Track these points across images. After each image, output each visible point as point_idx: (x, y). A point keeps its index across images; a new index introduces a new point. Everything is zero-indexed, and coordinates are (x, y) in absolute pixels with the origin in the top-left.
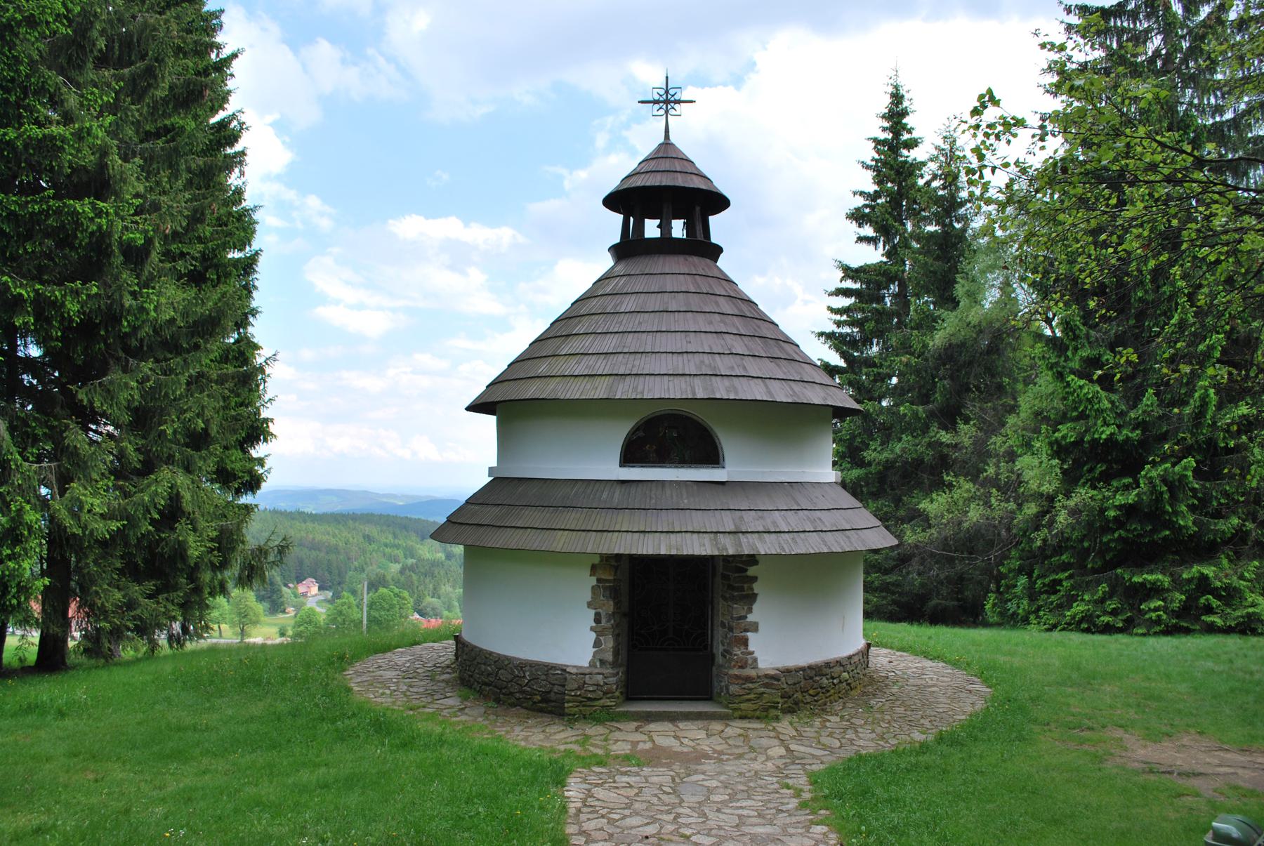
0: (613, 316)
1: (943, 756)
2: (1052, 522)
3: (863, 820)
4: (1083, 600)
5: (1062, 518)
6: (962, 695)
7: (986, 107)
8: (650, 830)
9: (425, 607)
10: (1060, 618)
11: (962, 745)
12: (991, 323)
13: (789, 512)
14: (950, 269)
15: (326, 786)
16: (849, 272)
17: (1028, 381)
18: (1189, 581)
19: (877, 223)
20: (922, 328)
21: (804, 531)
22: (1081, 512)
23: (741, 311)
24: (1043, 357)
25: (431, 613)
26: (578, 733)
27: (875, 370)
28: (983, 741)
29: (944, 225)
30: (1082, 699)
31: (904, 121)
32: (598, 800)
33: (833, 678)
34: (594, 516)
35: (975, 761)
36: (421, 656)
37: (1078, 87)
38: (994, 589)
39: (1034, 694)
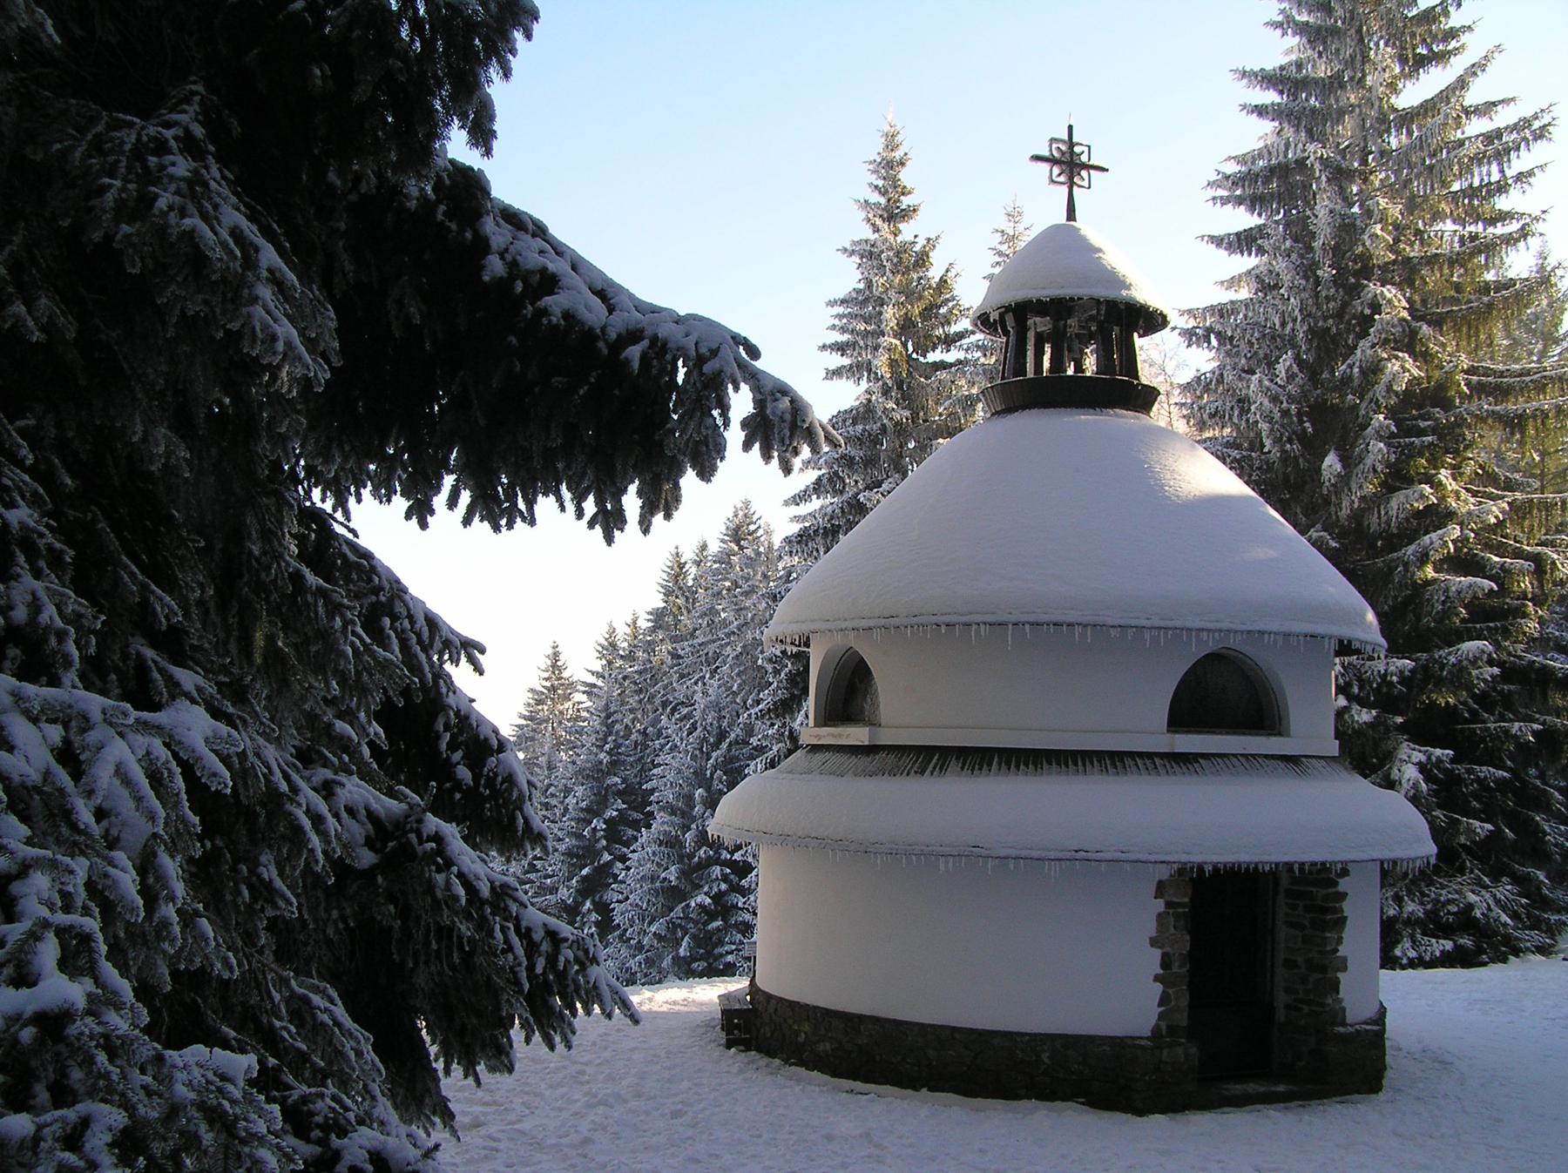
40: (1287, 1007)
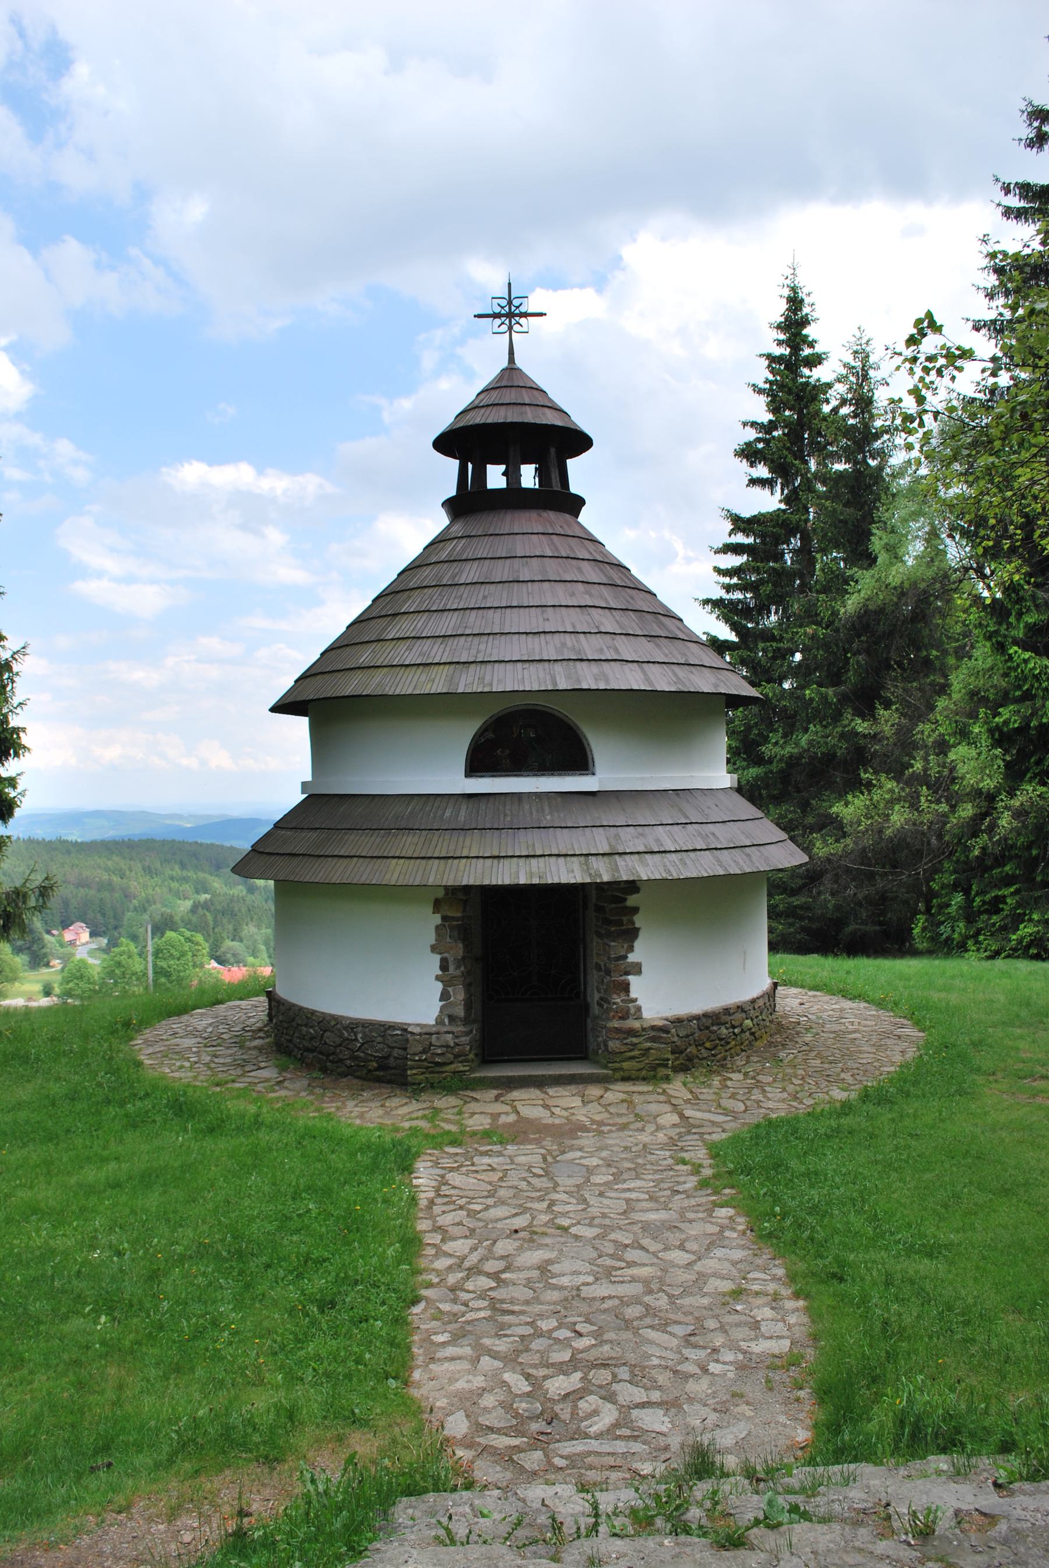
0: (450, 589)
1: (869, 1117)
2: (992, 828)
3: (776, 1199)
4: (1031, 920)
5: (1005, 821)
6: (889, 1042)
7: (925, 335)
8: (520, 1222)
9: (225, 953)
10: (1004, 943)
11: (892, 1102)
12: (915, 583)
13: (675, 827)
14: (864, 517)
15: (117, 1185)
16: (740, 524)
17: (962, 654)
19: (772, 461)
20: (831, 591)
21: (695, 850)
22: (1027, 813)
23: (611, 578)
24: (980, 624)
25: (232, 960)
26: (424, 1106)
27: (774, 644)
28: (917, 1097)
29: (856, 462)
30: (1034, 1042)
31: (804, 332)
32: (454, 1187)
33: (734, 1027)
34: (435, 838)
35: (907, 1122)
36: (225, 1018)
37: (1040, 311)
38: (923, 909)
39: (976, 1037)
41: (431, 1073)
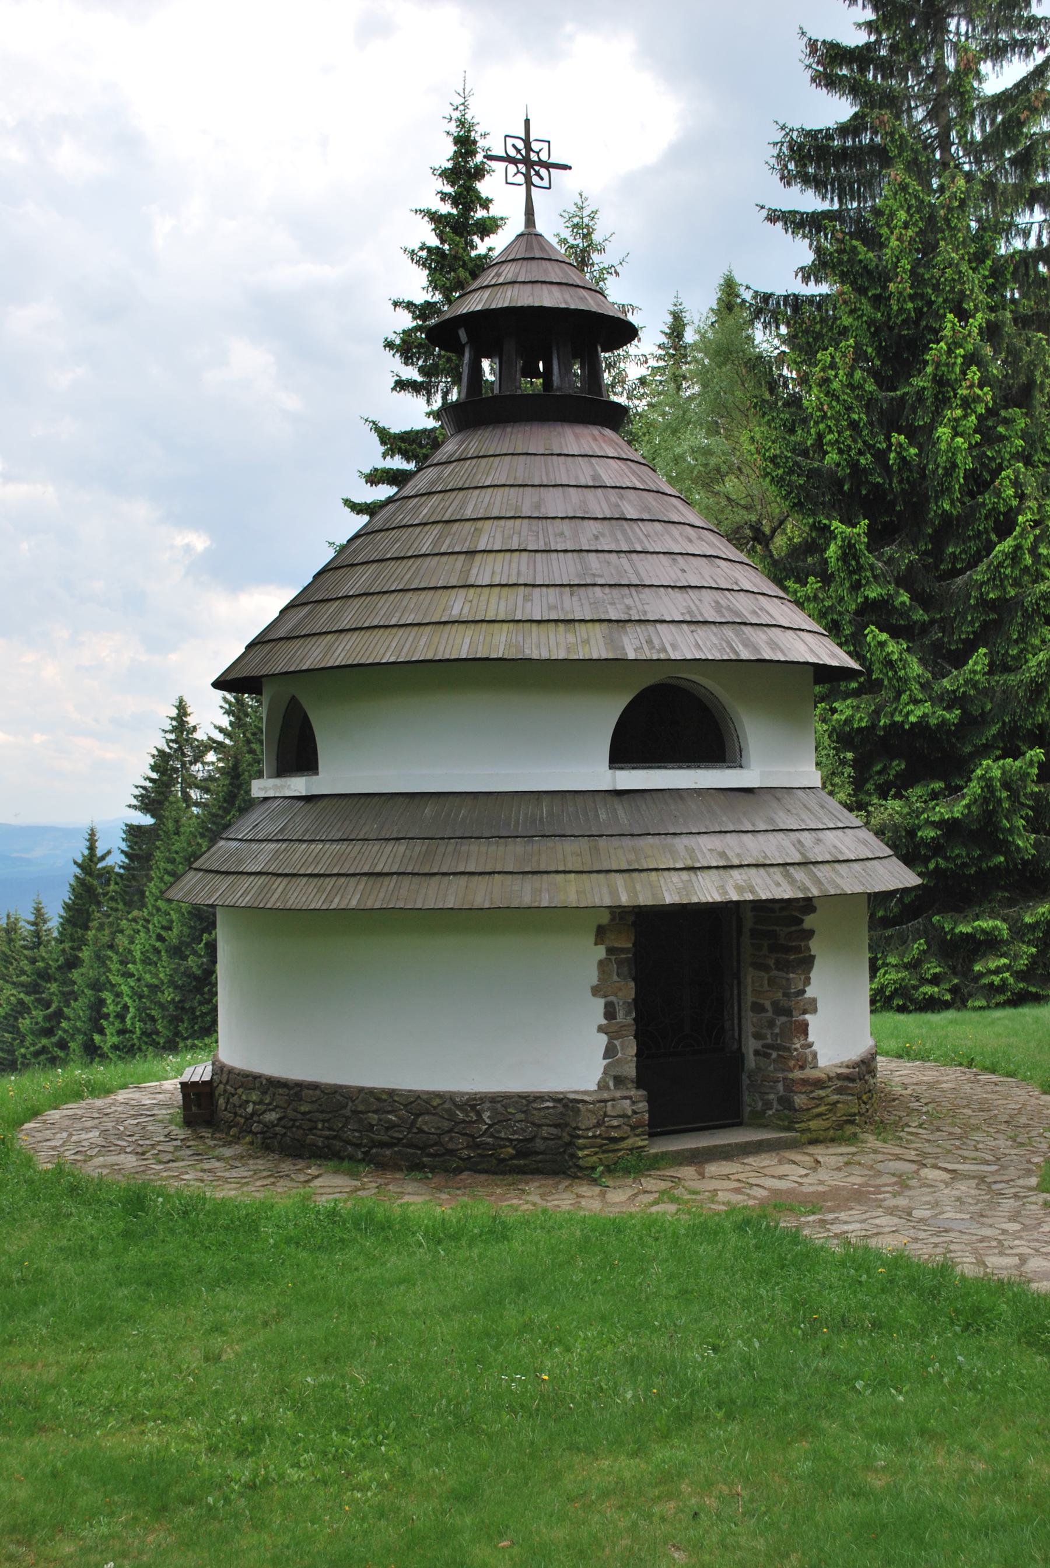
18: (1033, 927)
40: (757, 1053)
41: (604, 1152)
